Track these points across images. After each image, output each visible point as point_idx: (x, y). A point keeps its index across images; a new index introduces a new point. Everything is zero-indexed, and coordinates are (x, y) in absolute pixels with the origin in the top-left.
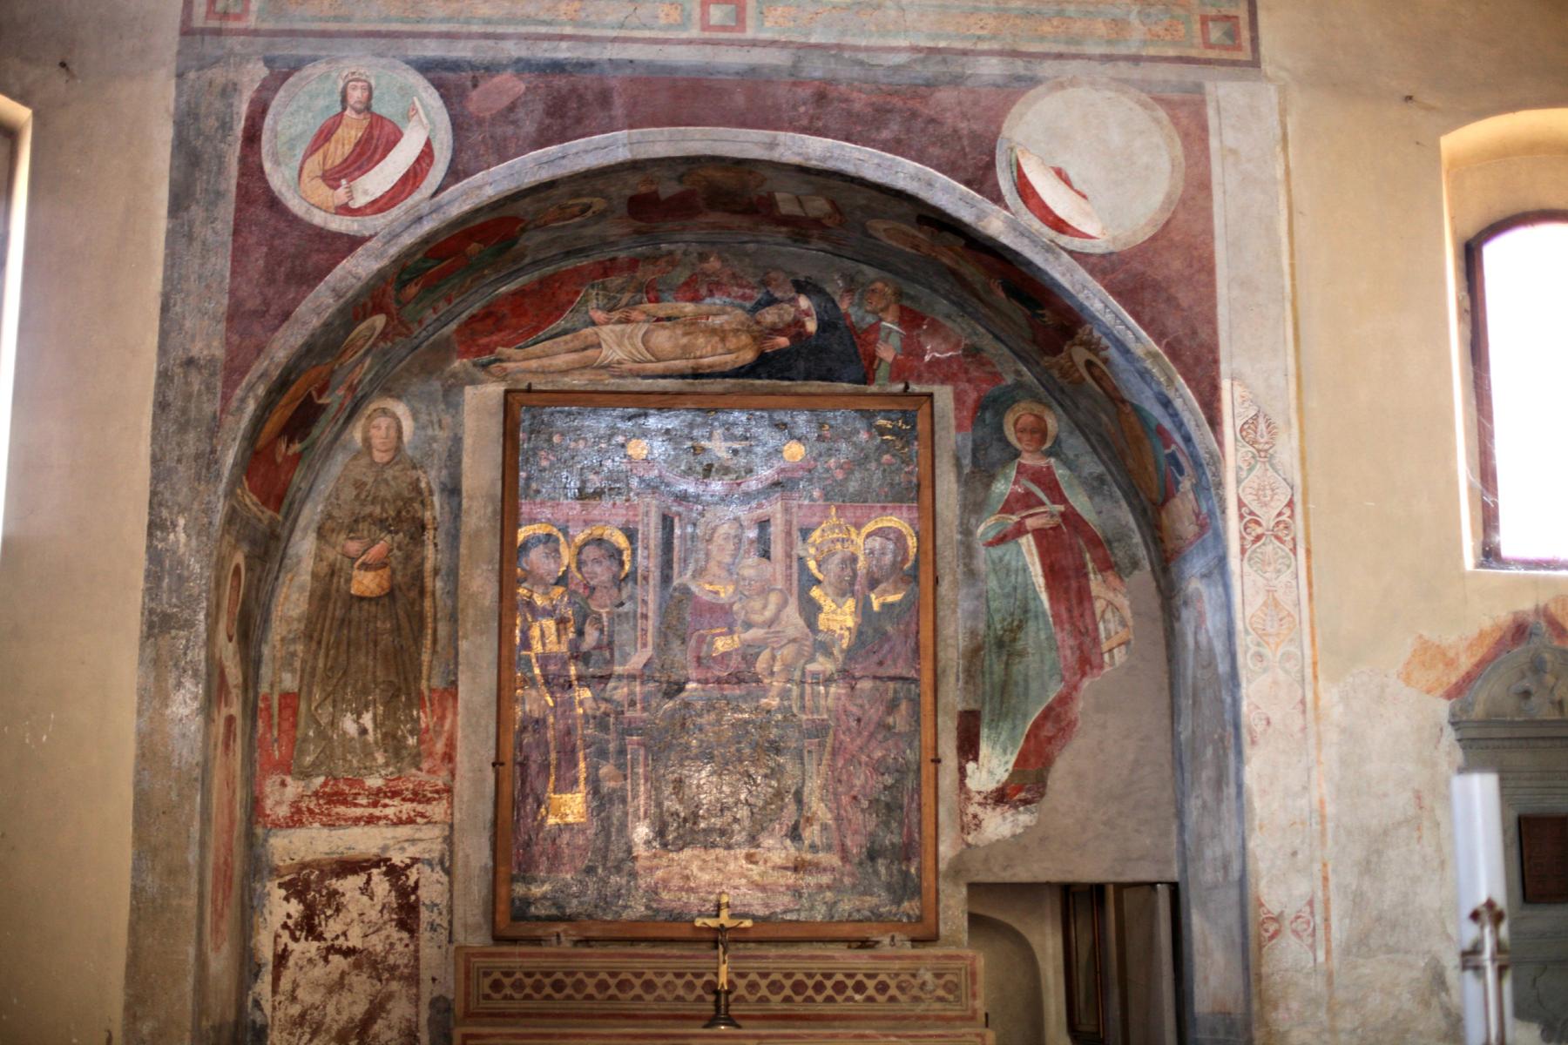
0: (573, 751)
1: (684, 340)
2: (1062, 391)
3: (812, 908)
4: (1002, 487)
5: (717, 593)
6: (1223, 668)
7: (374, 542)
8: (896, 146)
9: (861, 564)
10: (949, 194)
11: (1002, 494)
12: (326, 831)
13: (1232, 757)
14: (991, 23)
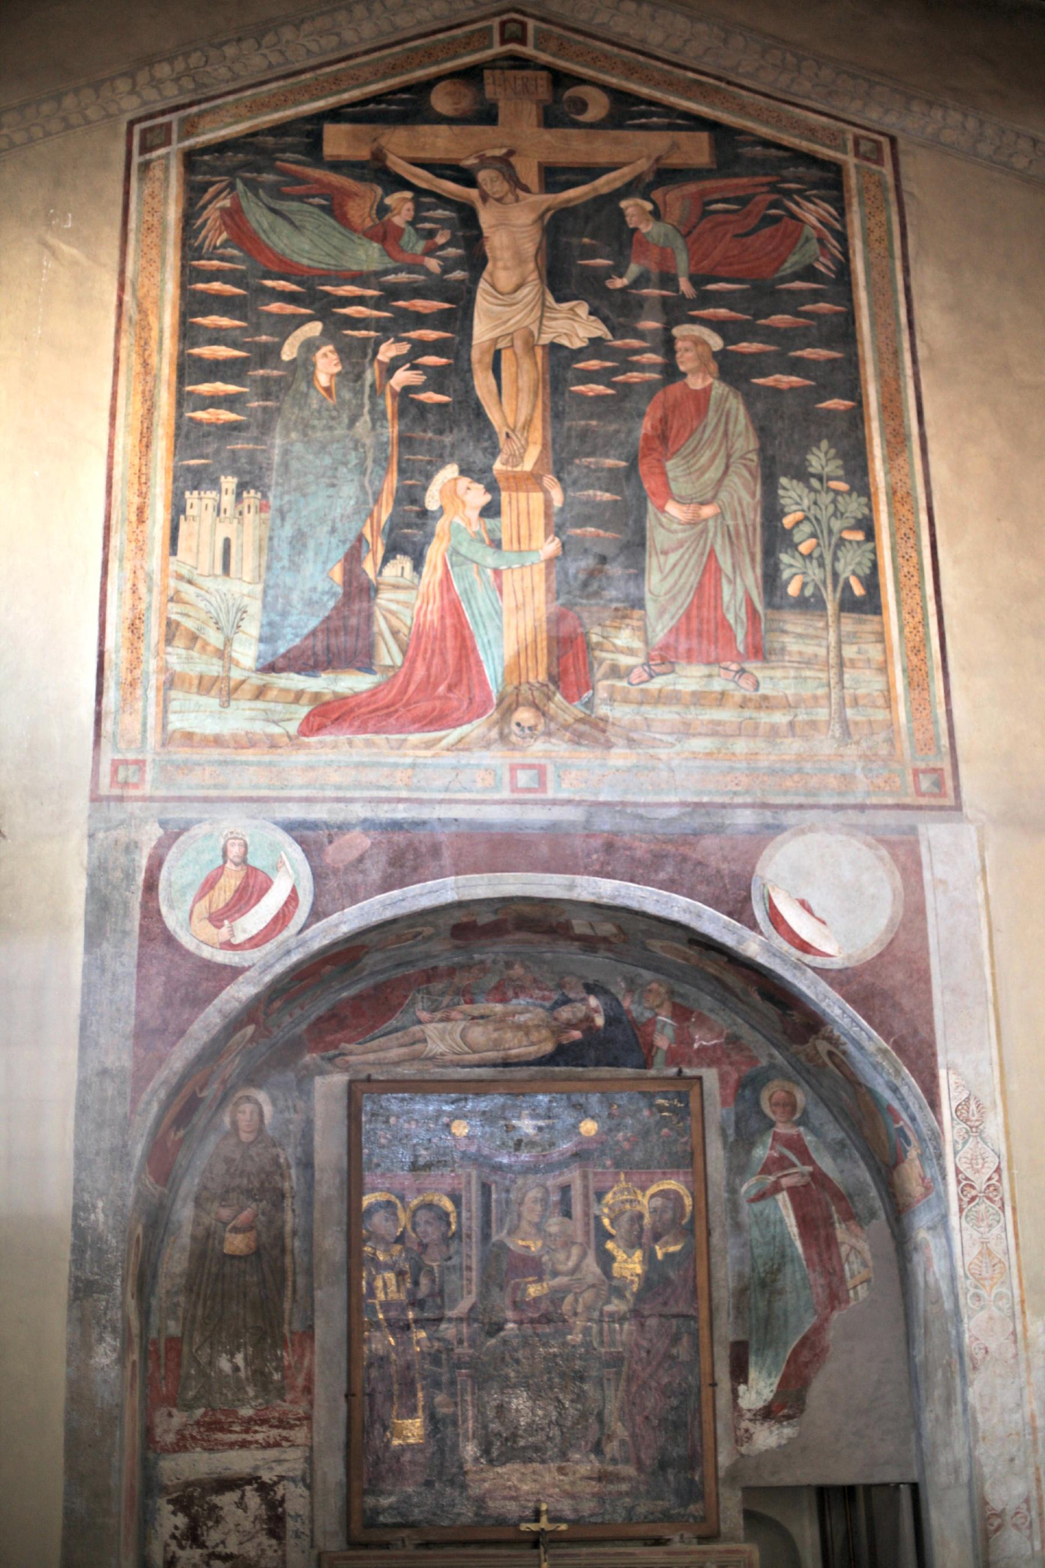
0: (412, 1383)
1: (495, 1035)
2: (808, 1071)
3: (614, 1512)
4: (761, 1153)
5: (528, 1247)
6: (948, 1305)
7: (242, 1209)
8: (671, 885)
9: (647, 1220)
10: (714, 924)
11: (761, 1159)
12: (206, 1455)
13: (958, 1380)
14: (745, 780)
